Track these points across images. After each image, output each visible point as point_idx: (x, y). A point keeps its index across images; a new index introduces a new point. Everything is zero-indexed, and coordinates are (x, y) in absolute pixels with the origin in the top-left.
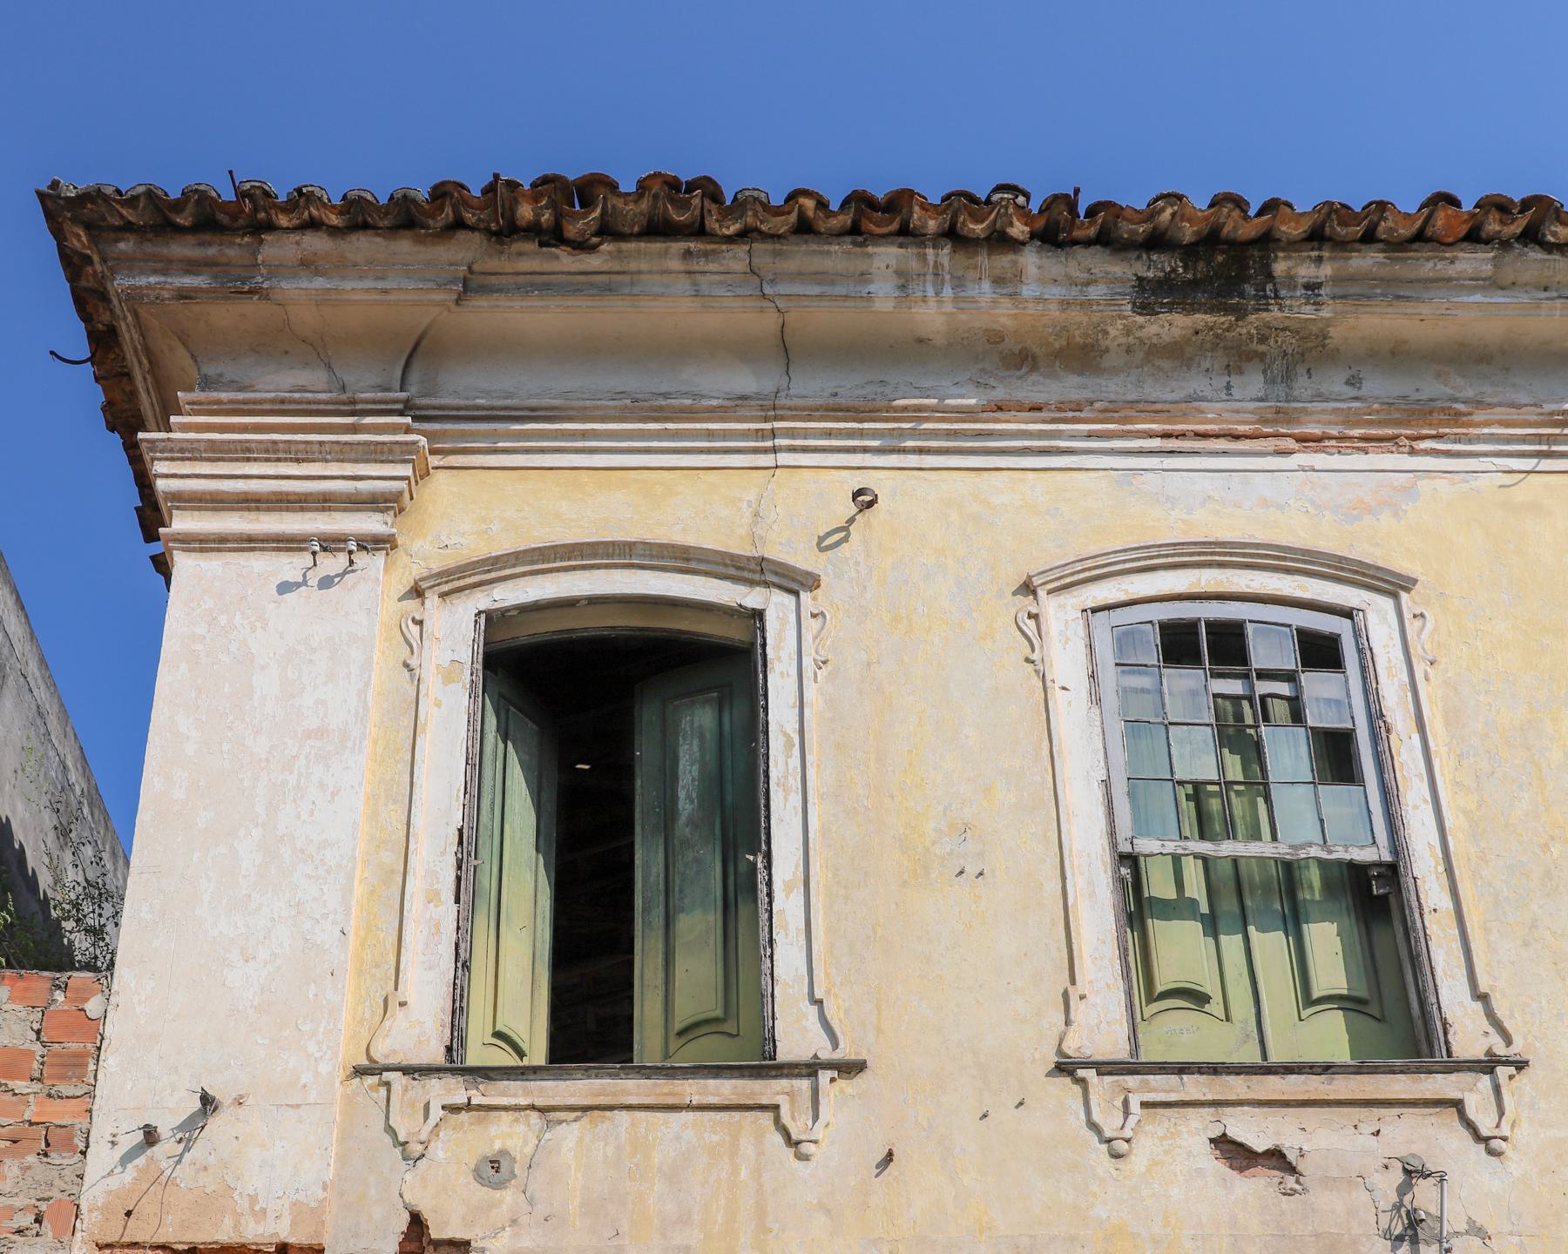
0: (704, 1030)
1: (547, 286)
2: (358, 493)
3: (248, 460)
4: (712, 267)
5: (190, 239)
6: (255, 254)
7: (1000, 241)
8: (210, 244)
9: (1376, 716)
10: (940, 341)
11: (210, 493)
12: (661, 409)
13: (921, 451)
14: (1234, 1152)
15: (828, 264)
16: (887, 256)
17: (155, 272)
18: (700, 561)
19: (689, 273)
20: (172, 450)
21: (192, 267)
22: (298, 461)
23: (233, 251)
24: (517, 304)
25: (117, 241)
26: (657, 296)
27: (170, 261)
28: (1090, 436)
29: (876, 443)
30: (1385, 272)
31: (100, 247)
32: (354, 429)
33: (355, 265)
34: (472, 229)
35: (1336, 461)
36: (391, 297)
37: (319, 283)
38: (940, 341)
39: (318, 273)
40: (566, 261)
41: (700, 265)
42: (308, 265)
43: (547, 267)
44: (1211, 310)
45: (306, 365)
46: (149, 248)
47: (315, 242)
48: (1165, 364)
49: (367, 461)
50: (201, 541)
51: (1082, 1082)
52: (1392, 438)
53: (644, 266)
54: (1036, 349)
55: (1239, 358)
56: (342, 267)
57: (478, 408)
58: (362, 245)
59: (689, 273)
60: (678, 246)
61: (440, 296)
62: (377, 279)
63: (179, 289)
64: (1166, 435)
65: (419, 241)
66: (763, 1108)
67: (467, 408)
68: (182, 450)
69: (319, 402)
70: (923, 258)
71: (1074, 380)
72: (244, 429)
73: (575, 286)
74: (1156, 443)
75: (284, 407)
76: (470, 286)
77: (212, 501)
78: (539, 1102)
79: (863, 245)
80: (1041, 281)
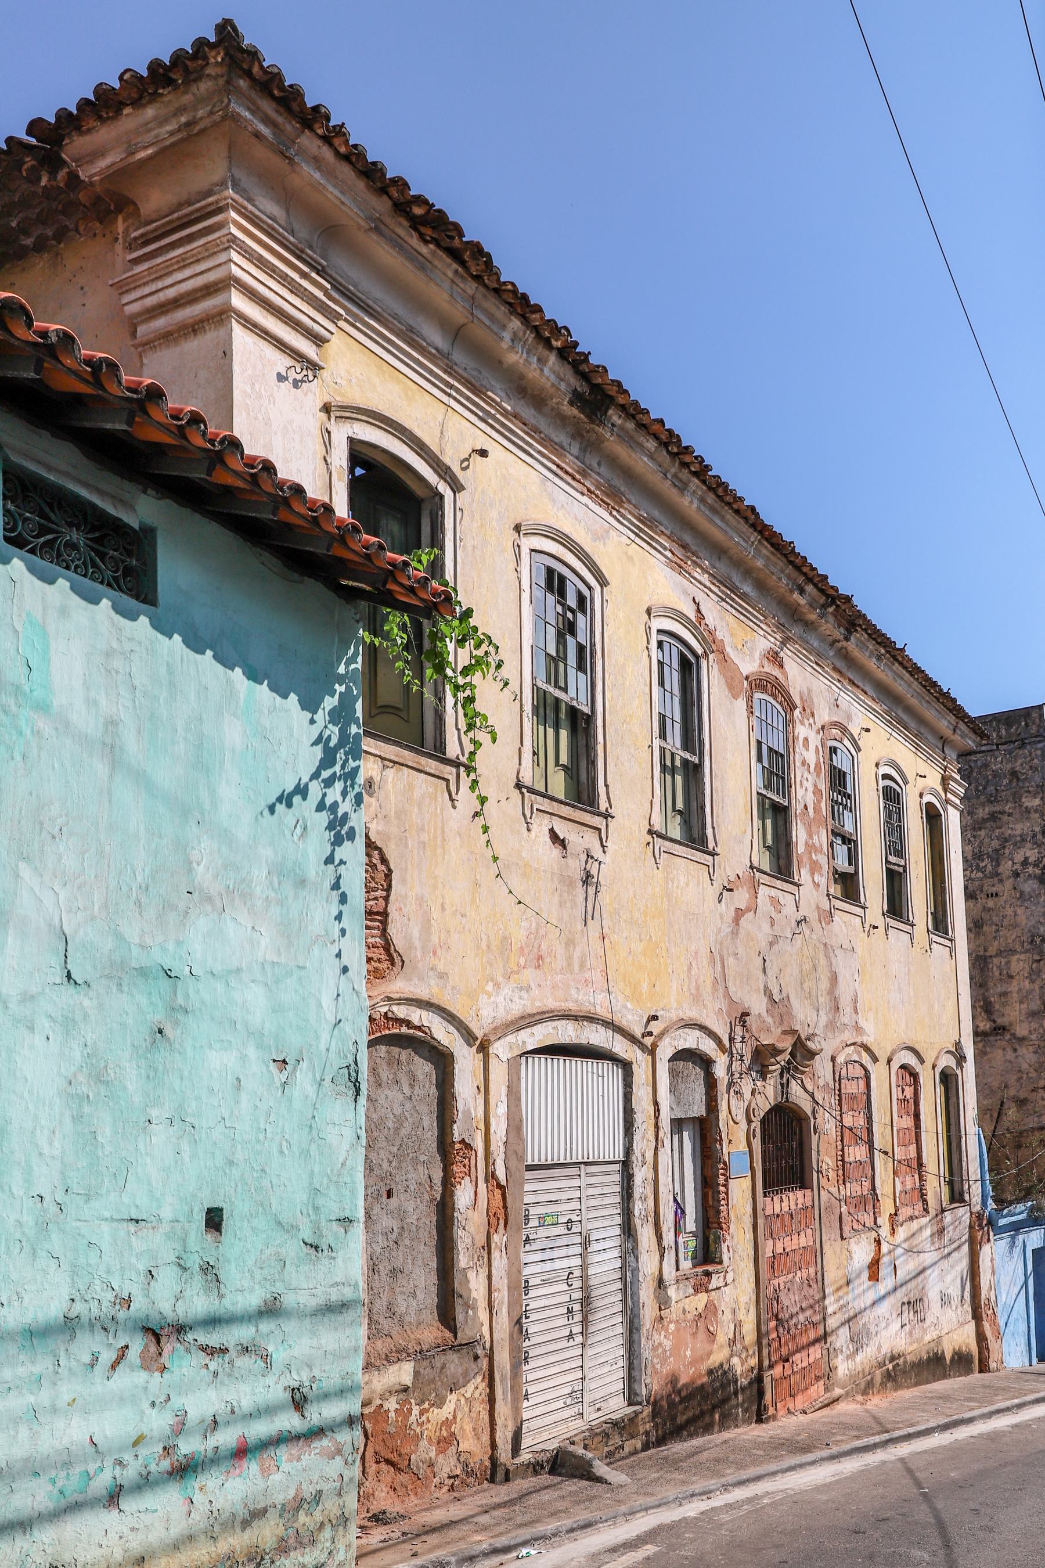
0: (388, 710)
1: (401, 247)
2: (312, 330)
3: (271, 276)
4: (462, 285)
5: (274, 105)
6: (298, 137)
7: (547, 343)
8: (281, 114)
9: (593, 645)
10: (505, 366)
11: (253, 289)
12: (414, 340)
13: (491, 426)
14: (554, 835)
15: (493, 310)
16: (516, 324)
17: (249, 109)
18: (426, 453)
19: (453, 281)
20: (241, 248)
21: (267, 121)
22: (292, 292)
23: (290, 127)
24: (387, 248)
25: (241, 77)
26: (437, 285)
27: (258, 108)
28: (540, 452)
29: (481, 414)
30: (632, 433)
31: (232, 75)
32: (304, 275)
33: (336, 178)
34: (390, 198)
35: (592, 505)
36: (344, 208)
37: (317, 175)
38: (505, 366)
39: (319, 168)
40: (415, 241)
41: (458, 281)
42: (317, 162)
43: (407, 238)
44: (587, 416)
45: (278, 202)
46: (253, 95)
47: (327, 153)
48: (558, 422)
49: (319, 311)
50: (245, 320)
51: (522, 794)
52: (608, 504)
53: (440, 266)
54: (529, 391)
55: (577, 434)
56: (329, 173)
57: (348, 290)
58: (345, 171)
59: (453, 281)
60: (455, 266)
61: (362, 223)
62: (342, 192)
63: (258, 131)
64: (558, 466)
65: (368, 187)
66: (444, 779)
67: (344, 287)
68: (245, 251)
69: (288, 240)
70: (525, 334)
71: (532, 411)
72: (260, 242)
73: (412, 257)
74: (554, 468)
75: (273, 233)
76: (378, 228)
77: (251, 293)
78: (383, 755)
79: (511, 313)
80: (550, 369)
